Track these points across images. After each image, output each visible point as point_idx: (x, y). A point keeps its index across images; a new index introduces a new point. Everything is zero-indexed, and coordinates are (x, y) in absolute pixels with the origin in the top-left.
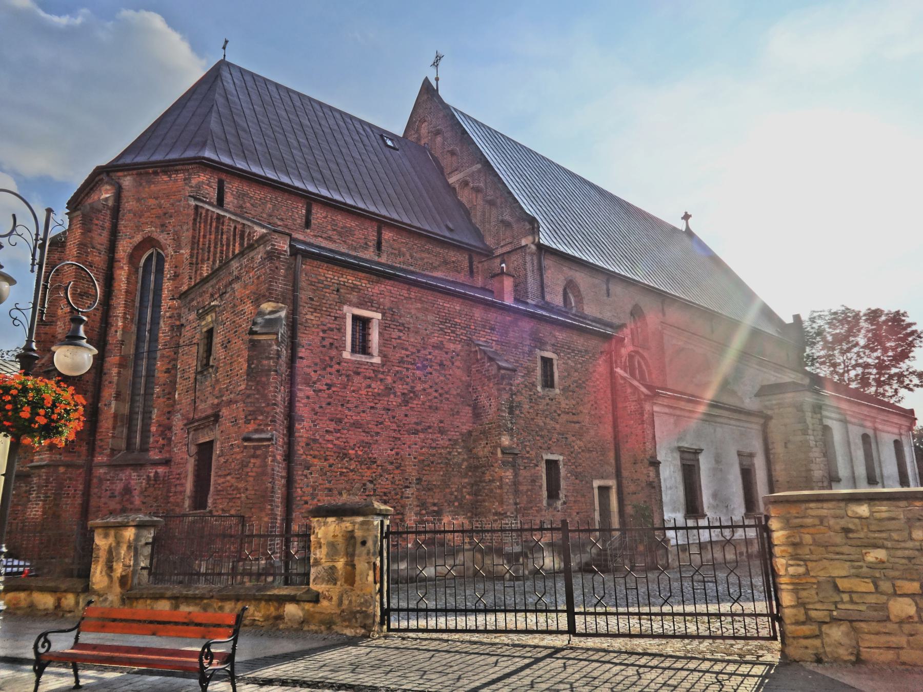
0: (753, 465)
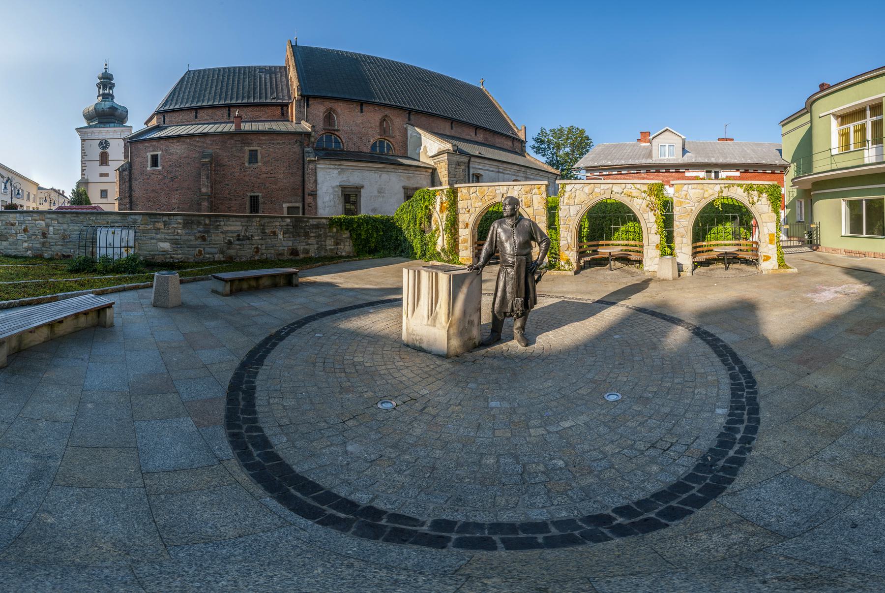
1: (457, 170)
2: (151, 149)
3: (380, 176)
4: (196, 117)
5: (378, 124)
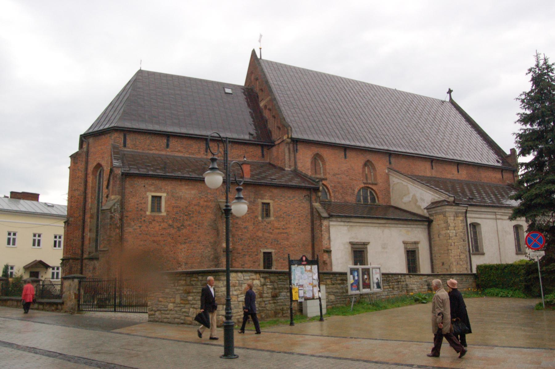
0: (418, 248)
1: (456, 222)
2: (152, 188)
3: (383, 231)
4: (168, 146)
5: (361, 171)
